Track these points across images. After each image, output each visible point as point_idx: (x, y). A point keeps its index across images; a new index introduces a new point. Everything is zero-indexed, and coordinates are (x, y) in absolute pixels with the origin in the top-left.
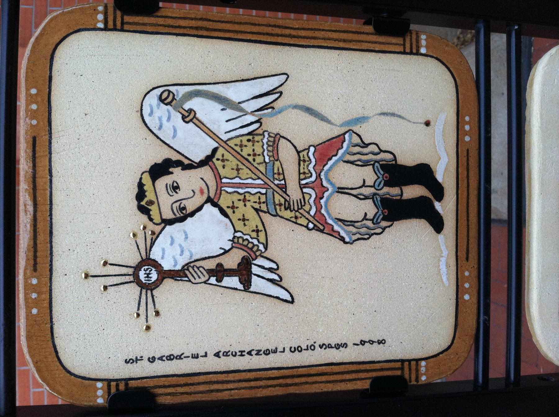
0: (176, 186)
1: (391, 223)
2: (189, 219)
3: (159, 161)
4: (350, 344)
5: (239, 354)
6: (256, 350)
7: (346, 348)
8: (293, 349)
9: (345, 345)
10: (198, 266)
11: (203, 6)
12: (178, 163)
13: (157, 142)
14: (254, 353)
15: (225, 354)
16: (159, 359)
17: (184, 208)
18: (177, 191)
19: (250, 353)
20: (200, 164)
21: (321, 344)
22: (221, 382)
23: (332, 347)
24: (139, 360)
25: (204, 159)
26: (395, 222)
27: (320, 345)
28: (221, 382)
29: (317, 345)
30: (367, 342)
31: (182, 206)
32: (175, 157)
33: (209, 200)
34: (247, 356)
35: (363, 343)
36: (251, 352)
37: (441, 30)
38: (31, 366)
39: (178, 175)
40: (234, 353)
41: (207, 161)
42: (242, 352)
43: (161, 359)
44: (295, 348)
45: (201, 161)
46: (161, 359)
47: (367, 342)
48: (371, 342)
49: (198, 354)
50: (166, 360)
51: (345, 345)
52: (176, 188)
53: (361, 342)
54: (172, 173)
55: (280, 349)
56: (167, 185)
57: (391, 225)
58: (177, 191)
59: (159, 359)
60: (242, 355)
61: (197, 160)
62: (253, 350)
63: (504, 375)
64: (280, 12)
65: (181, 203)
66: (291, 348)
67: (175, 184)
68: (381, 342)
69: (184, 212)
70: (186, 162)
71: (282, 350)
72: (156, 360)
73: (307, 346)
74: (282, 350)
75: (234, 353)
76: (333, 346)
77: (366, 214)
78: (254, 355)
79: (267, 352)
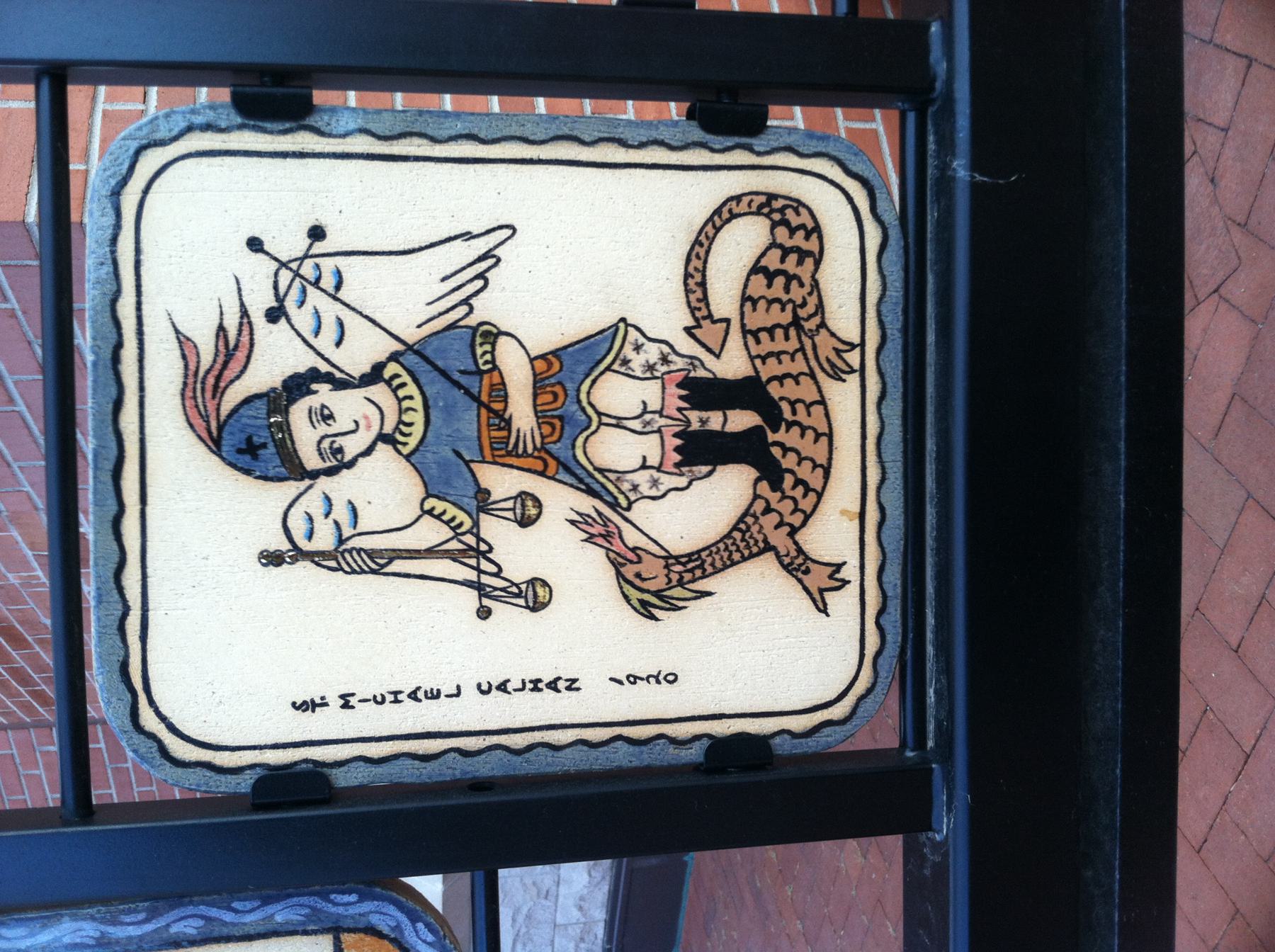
1: (709, 468)
2: (345, 471)
3: (302, 370)
4: (470, 692)
5: (390, 698)
6: (567, 680)
8: (485, 687)
10: (793, 398)
11: (404, 94)
12: (328, 378)
14: (561, 685)
16: (498, 688)
17: (340, 450)
19: (553, 685)
20: (365, 379)
25: (369, 371)
26: (719, 468)
30: (642, 679)
31: (336, 446)
32: (324, 367)
33: (383, 438)
34: (409, 703)
35: (633, 679)
38: (102, 745)
39: (324, 394)
40: (379, 699)
41: (374, 375)
42: (396, 693)
45: (363, 376)
47: (642, 679)
49: (438, 691)
50: (544, 688)
53: (628, 677)
54: (315, 392)
55: (449, 689)
56: (311, 407)
57: (710, 474)
59: (498, 688)
60: (396, 701)
61: (357, 374)
62: (559, 678)
64: (541, 96)
65: (706, 233)
66: (479, 686)
67: (326, 412)
68: (672, 679)
69: (339, 457)
70: (338, 375)
75: (379, 699)
77: (644, 458)
78: (563, 690)
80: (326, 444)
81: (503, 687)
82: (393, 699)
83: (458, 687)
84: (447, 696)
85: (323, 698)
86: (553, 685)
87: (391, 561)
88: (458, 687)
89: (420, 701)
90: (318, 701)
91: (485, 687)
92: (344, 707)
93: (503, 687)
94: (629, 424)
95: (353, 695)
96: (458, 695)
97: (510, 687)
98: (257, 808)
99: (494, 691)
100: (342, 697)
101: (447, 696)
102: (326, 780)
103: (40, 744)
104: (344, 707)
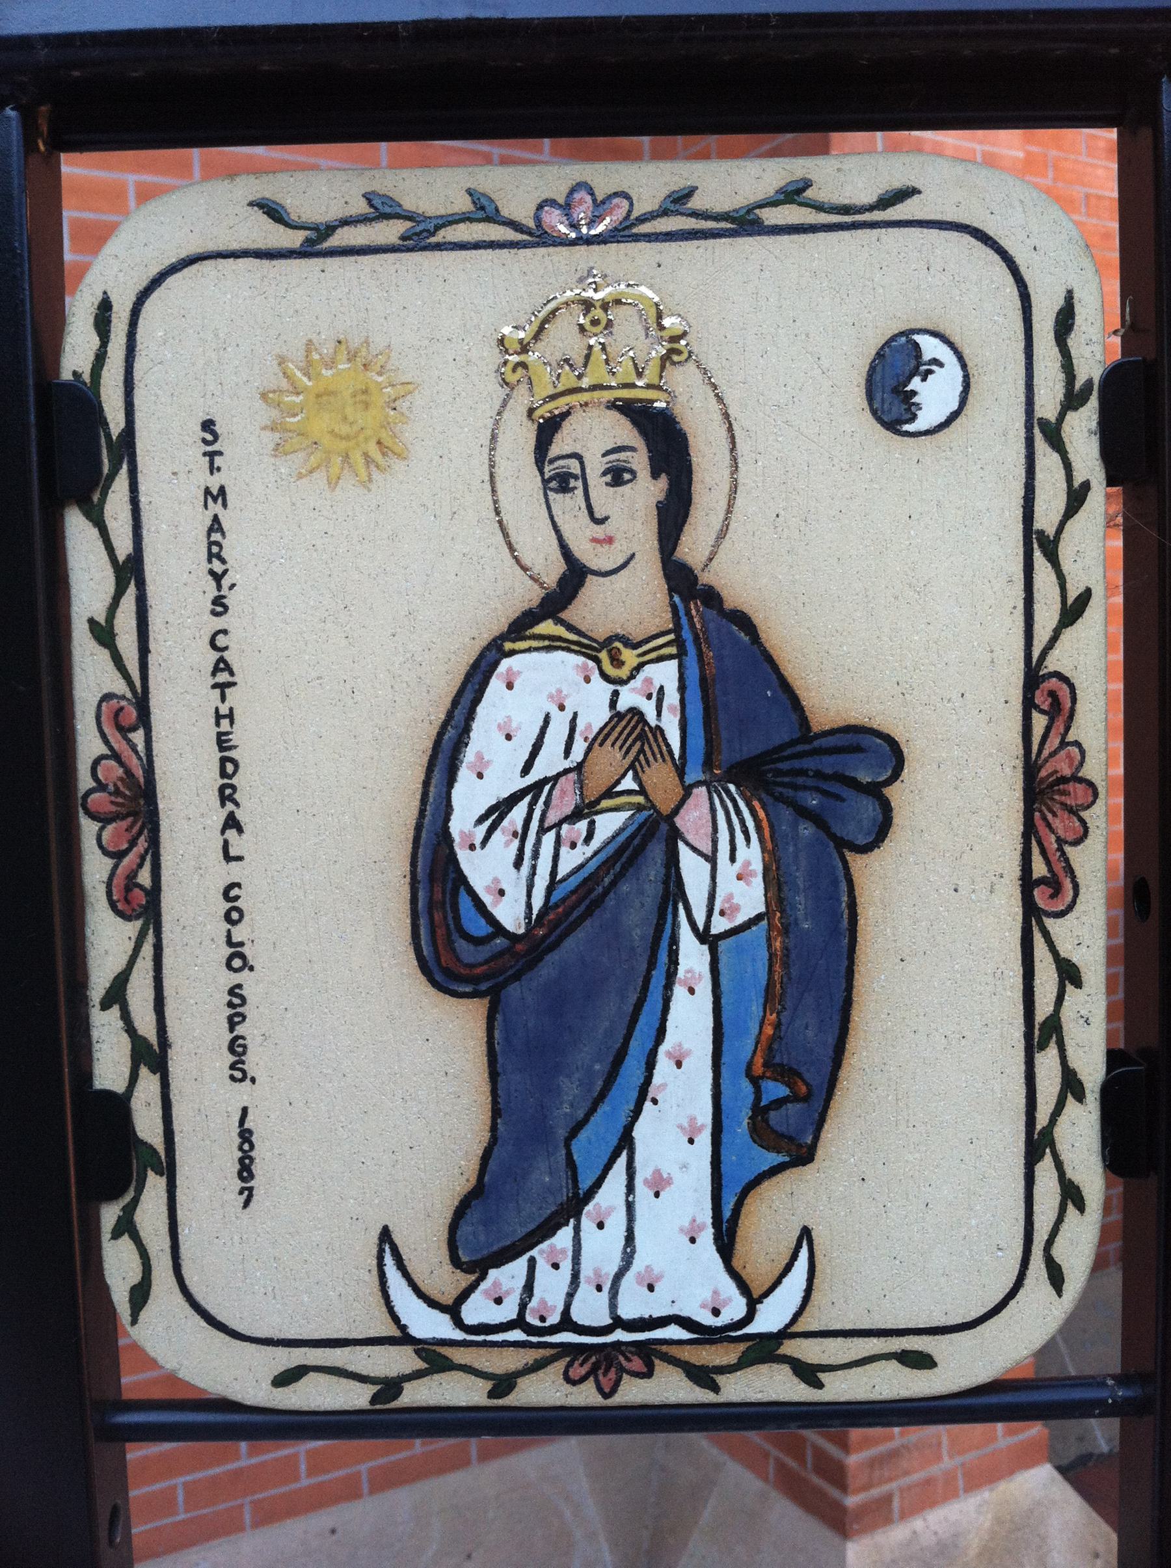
0: (568, 483)
7: (232, 1078)
8: (221, 641)
9: (239, 1072)
13: (1053, 352)
15: (215, 549)
16: (221, 660)
18: (608, 478)
21: (243, 992)
22: (455, 150)
23: (232, 1026)
24: (212, 463)
27: (239, 986)
28: (455, 150)
29: (243, 977)
36: (231, 827)
37: (1122, 1035)
38: (243, 1463)
43: (216, 525)
44: (237, 898)
46: (216, 525)
48: (220, 605)
51: (239, 1072)
52: (617, 476)
58: (608, 478)
59: (216, 519)
63: (127, 1395)
66: (238, 885)
71: (234, 940)
72: (229, 926)
73: (241, 944)
74: (233, 852)
76: (240, 1030)
79: (239, 1046)
80: (574, 466)
81: (232, 823)
82: (227, 721)
83: (239, 859)
84: (229, 931)
85: (219, 469)
86: (222, 665)
87: (438, 228)
88: (239, 859)
89: (214, 674)
90: (218, 461)
91: (233, 893)
92: (207, 492)
93: (232, 823)
94: (771, 216)
95: (225, 505)
96: (228, 858)
97: (231, 834)
98: (37, 386)
99: (217, 655)
100: (222, 490)
101: (229, 931)
102: (113, 1195)
103: (255, 1503)
104: (207, 492)
